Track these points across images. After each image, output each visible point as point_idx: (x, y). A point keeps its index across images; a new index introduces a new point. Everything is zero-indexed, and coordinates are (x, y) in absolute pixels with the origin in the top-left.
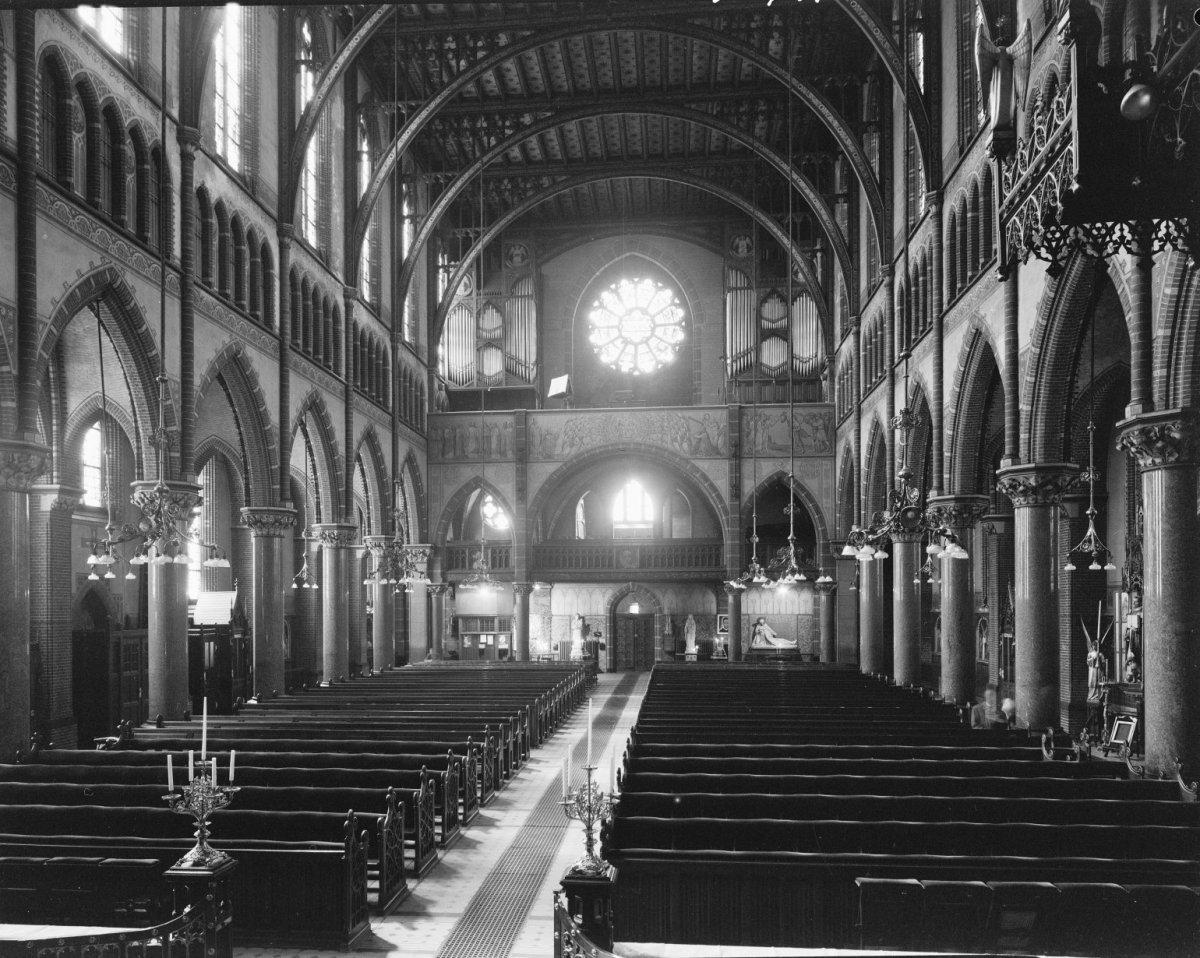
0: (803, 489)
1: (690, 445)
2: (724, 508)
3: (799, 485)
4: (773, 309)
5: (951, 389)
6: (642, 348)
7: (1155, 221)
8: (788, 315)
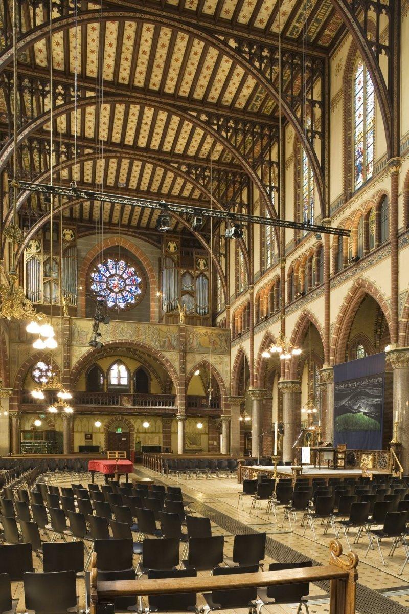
0: (216, 370)
1: (160, 343)
2: (177, 377)
3: (214, 369)
4: (187, 284)
5: (337, 314)
6: (120, 295)
7: (158, 525)
8: (195, 285)
